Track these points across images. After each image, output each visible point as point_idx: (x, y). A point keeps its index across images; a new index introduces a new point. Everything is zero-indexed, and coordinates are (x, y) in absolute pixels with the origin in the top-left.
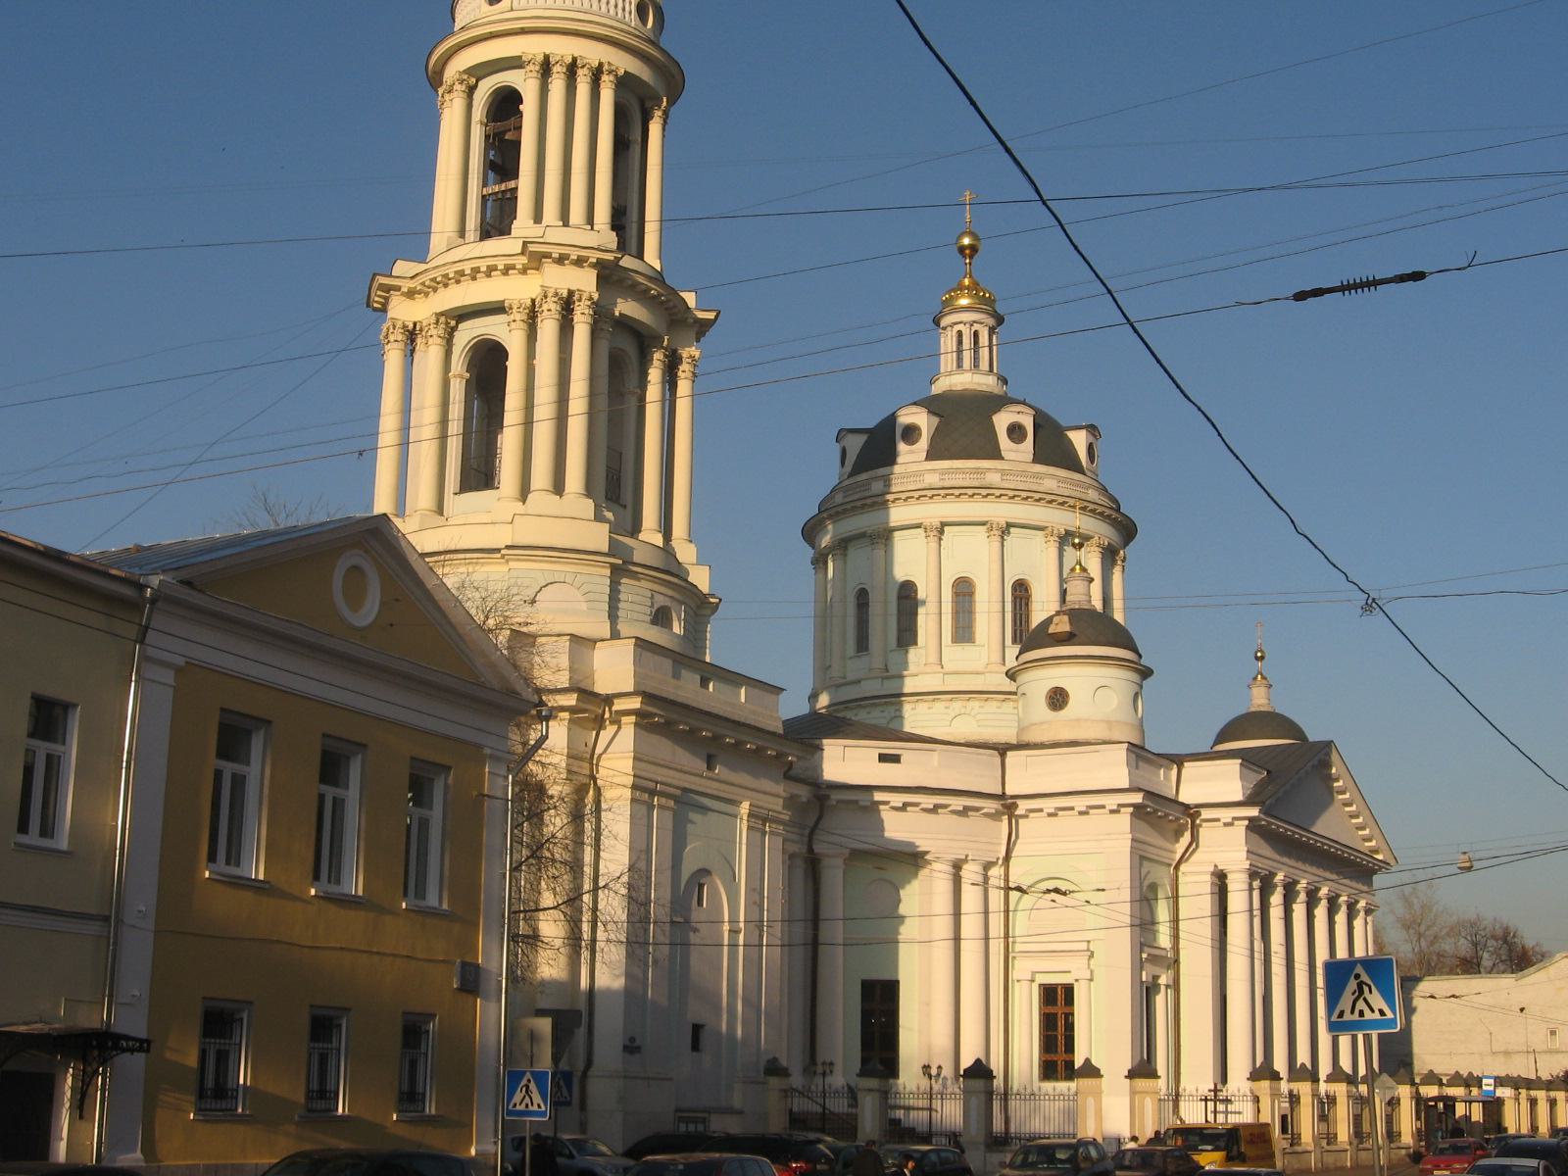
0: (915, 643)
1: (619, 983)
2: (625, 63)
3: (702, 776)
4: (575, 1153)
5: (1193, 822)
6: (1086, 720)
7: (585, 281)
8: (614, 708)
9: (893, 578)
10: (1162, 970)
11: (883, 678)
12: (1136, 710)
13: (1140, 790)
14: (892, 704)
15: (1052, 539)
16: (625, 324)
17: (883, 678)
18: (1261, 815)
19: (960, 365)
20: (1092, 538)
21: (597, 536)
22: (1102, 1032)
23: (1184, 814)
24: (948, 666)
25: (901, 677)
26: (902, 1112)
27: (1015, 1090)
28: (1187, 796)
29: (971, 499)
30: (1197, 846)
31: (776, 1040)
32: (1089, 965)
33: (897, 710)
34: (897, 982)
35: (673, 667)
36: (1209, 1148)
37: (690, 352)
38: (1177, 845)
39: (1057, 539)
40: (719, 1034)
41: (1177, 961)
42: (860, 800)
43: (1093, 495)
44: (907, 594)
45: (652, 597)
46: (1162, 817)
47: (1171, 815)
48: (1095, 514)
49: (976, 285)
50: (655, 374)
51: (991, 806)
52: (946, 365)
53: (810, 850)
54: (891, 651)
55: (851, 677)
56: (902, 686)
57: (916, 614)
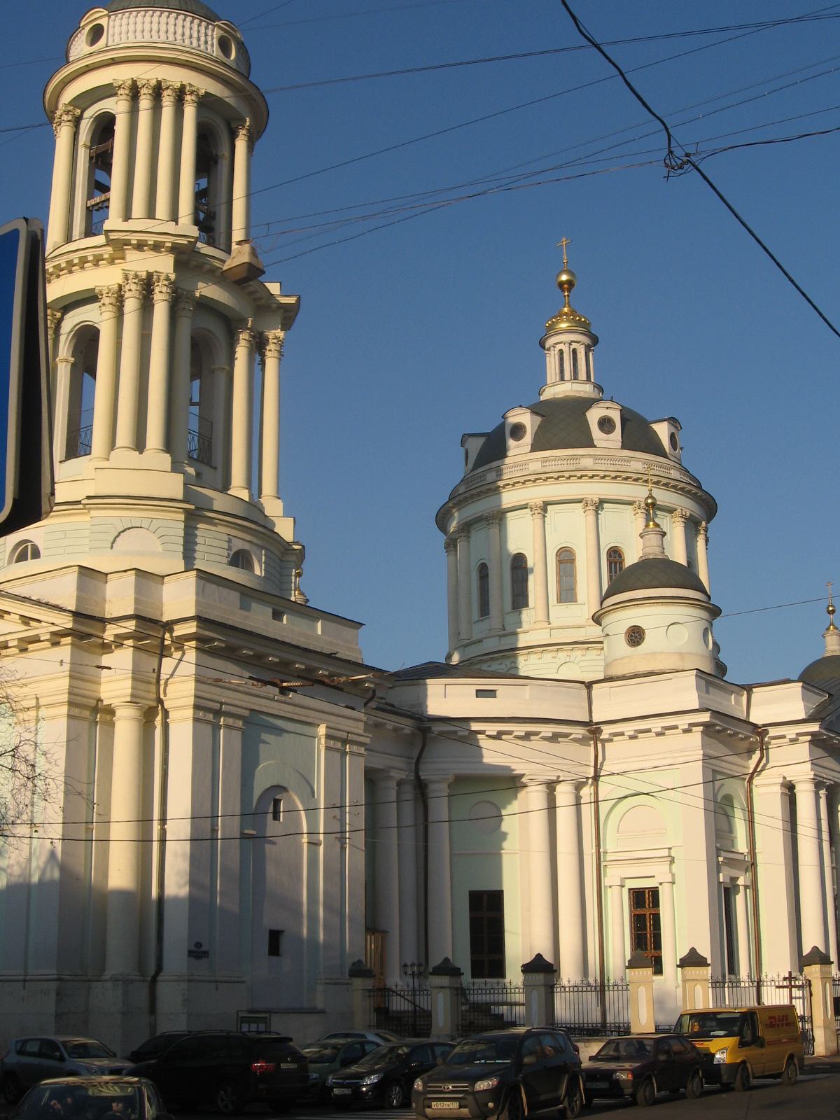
0: (526, 605)
1: (184, 891)
2: (205, 85)
3: (273, 699)
4: (66, 1055)
5: (762, 740)
6: (661, 653)
7: (164, 264)
8: (175, 634)
9: (507, 551)
10: (740, 872)
11: (500, 636)
12: (707, 645)
13: (707, 710)
14: (508, 657)
15: (639, 511)
16: (205, 305)
17: (500, 636)
18: (823, 731)
19: (562, 379)
20: (676, 510)
21: (173, 485)
22: (686, 925)
23: (752, 733)
24: (555, 622)
25: (516, 634)
26: (505, 1007)
27: (612, 982)
28: (757, 717)
29: (568, 481)
30: (768, 761)
31: (354, 943)
32: (670, 869)
33: (513, 662)
34: (502, 891)
35: (241, 601)
36: (722, 1033)
37: (275, 334)
38: (750, 761)
39: (643, 511)
40: (300, 938)
41: (754, 864)
42: (459, 732)
43: (675, 474)
44: (519, 565)
45: (229, 541)
46: (731, 738)
47: (739, 733)
48: (678, 490)
49: (573, 312)
50: (241, 352)
51: (579, 732)
52: (551, 379)
53: (417, 776)
54: (507, 613)
55: (476, 637)
56: (517, 640)
57: (526, 581)
